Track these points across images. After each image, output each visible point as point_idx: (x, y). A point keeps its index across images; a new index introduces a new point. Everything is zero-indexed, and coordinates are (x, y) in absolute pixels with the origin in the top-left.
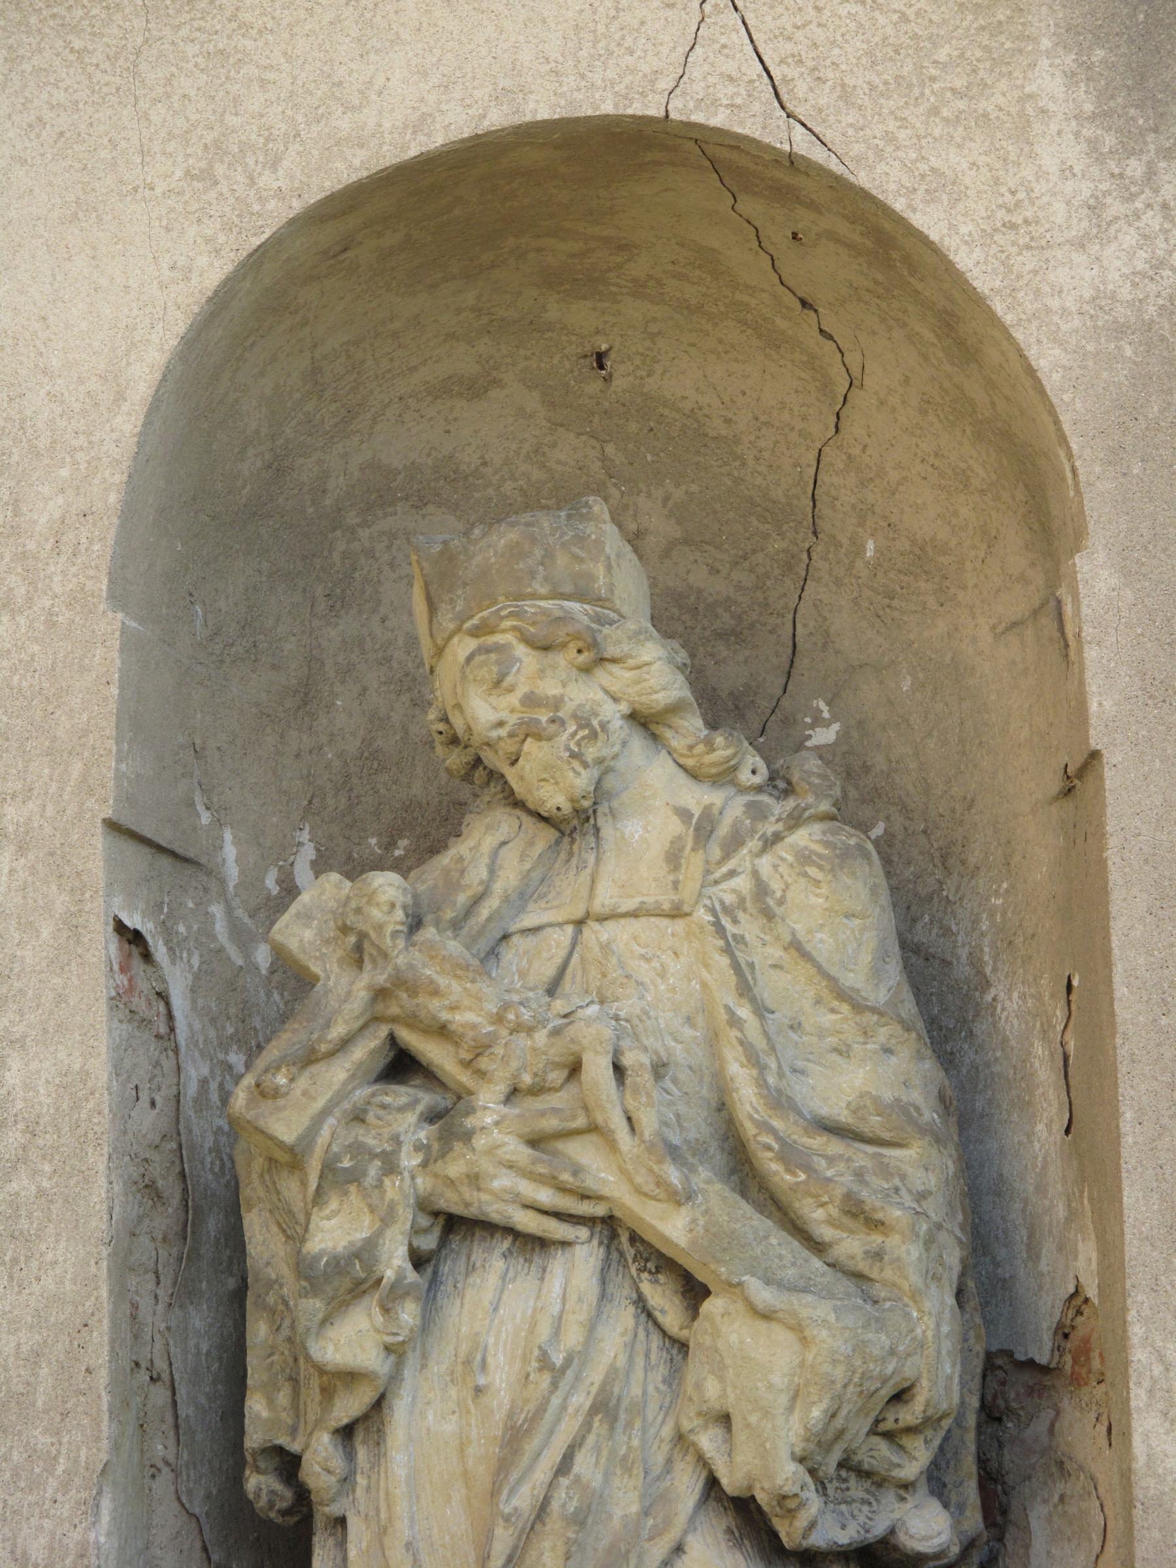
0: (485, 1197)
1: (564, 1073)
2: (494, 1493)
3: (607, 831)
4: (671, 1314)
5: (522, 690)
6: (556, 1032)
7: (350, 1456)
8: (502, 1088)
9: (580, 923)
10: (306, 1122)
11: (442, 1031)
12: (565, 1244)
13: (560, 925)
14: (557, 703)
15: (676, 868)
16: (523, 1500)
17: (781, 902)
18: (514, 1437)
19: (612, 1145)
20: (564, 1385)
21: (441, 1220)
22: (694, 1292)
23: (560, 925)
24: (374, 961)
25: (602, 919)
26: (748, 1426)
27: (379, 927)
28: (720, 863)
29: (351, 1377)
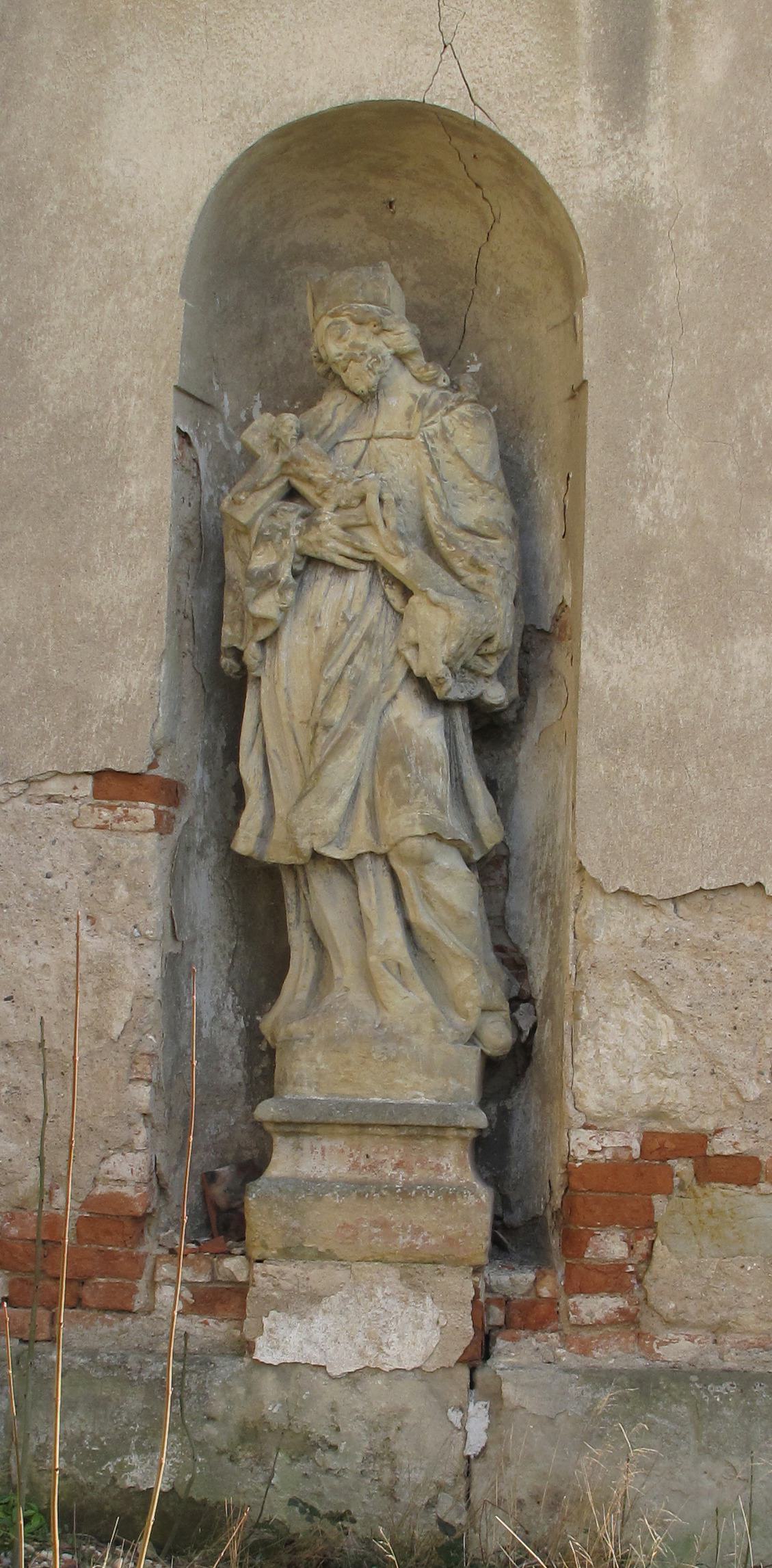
2: (321, 670)
3: (382, 401)
4: (397, 602)
5: (350, 341)
6: (356, 484)
8: (332, 506)
11: (309, 481)
14: (364, 347)
17: (452, 435)
22: (407, 593)
25: (378, 438)
29: (265, 620)
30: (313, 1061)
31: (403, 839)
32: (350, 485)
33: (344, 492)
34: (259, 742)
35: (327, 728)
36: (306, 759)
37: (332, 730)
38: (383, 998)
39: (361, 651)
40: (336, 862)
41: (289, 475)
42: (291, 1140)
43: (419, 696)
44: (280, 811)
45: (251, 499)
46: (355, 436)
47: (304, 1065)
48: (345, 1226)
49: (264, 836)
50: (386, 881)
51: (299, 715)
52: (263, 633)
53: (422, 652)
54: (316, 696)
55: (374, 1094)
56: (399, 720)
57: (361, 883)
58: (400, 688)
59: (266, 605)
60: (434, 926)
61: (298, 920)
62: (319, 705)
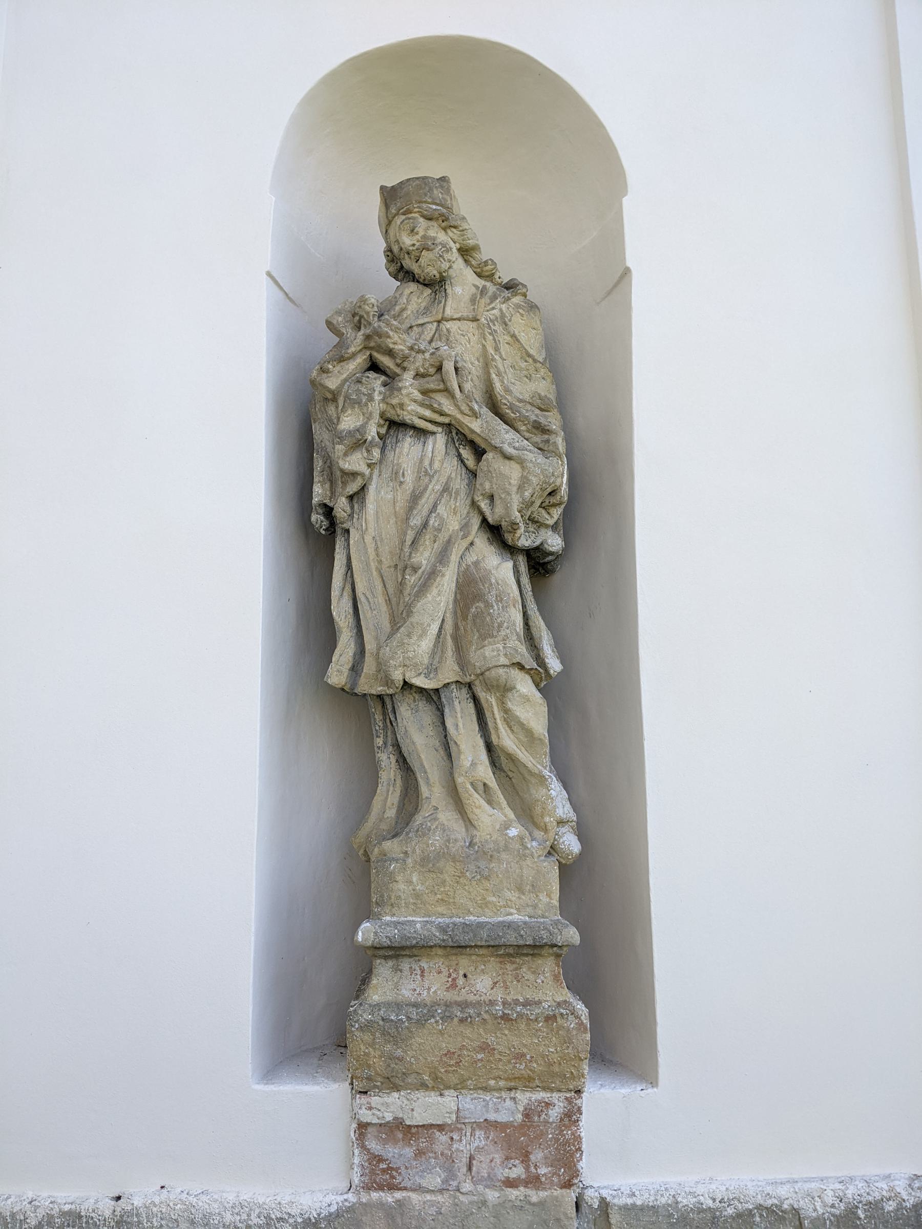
0: (405, 413)
1: (435, 370)
2: (408, 519)
3: (449, 291)
4: (471, 463)
5: (421, 233)
6: (432, 354)
7: (352, 508)
8: (412, 373)
9: (439, 322)
10: (339, 382)
11: (390, 353)
12: (434, 433)
13: (431, 322)
14: (434, 239)
15: (475, 304)
16: (416, 521)
17: (510, 321)
18: (415, 499)
19: (452, 396)
20: (433, 482)
21: (387, 423)
22: (479, 453)
23: (431, 322)
24: (365, 326)
25: (447, 321)
26: (501, 498)
27: (368, 313)
28: (489, 304)
29: (354, 475)
30: (410, 882)
31: (489, 669)
32: (427, 355)
33: (419, 362)
34: (348, 588)
35: (415, 570)
36: (394, 600)
37: (420, 571)
38: (471, 816)
39: (443, 501)
40: (421, 690)
41: (371, 348)
42: (390, 963)
43: (492, 544)
44: (370, 645)
45: (338, 368)
46: (426, 320)
47: (402, 886)
48: (449, 1054)
49: (356, 669)
50: (471, 707)
51: (387, 562)
52: (353, 487)
53: (497, 501)
54: (403, 542)
55: (469, 913)
56: (476, 563)
57: (447, 710)
58: (476, 536)
59: (355, 462)
60: (515, 748)
61: (385, 743)
62: (407, 550)
